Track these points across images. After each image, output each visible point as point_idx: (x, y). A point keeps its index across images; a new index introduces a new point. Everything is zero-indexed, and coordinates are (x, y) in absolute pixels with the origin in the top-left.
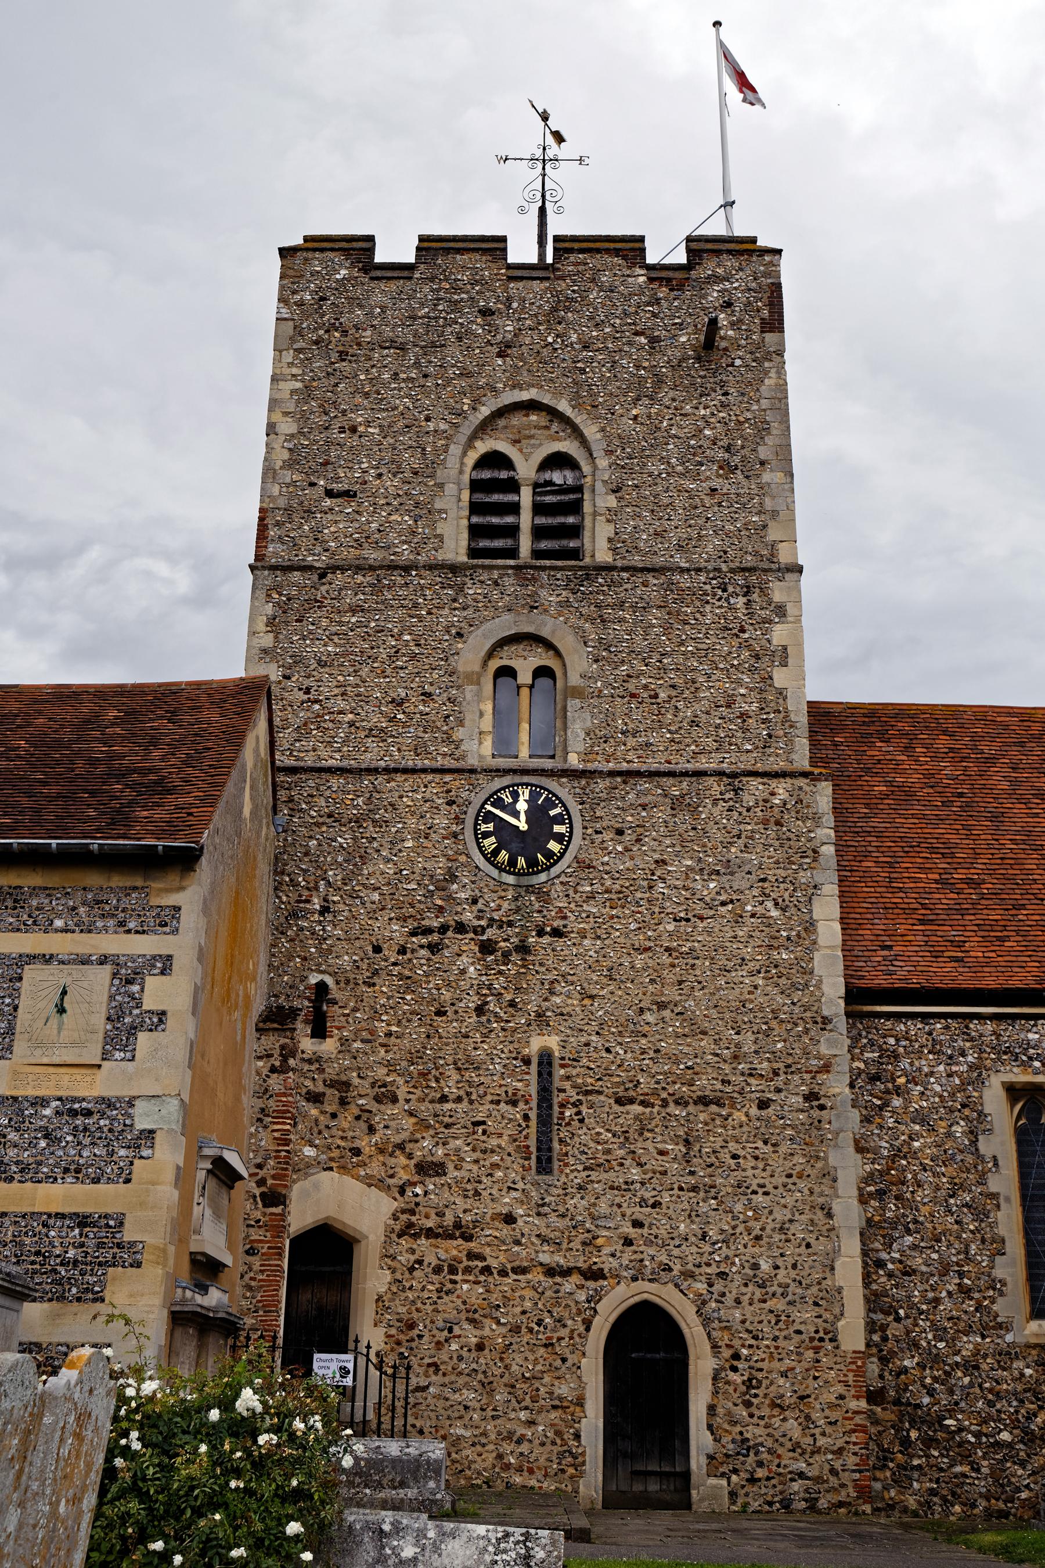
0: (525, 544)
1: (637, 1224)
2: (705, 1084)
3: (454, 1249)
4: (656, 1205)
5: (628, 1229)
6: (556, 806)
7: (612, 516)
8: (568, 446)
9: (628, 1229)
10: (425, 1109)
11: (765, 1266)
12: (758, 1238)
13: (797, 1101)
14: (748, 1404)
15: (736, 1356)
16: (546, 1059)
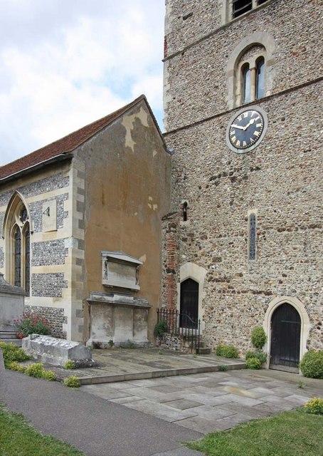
1: (284, 276)
2: (313, 220)
3: (223, 285)
5: (281, 278)
9: (281, 278)
10: (215, 240)
16: (253, 218)
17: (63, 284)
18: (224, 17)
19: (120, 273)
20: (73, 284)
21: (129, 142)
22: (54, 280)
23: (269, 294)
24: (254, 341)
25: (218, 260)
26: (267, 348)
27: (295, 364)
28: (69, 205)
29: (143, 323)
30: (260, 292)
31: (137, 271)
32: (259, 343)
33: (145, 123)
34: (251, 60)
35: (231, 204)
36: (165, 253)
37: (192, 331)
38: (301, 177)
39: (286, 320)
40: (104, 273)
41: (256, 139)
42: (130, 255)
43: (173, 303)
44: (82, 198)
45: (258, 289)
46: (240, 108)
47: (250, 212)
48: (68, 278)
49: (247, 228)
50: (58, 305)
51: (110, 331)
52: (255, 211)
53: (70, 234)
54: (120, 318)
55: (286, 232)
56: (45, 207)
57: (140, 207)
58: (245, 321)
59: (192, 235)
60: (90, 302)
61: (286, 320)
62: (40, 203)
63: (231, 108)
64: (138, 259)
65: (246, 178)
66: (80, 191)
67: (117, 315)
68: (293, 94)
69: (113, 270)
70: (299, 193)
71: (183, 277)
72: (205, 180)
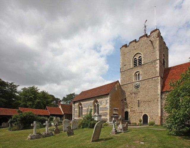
0: (138, 65)
3: (134, 112)
6: (157, 79)
7: (143, 60)
8: (140, 55)
10: (131, 104)
16: (139, 100)
17: (107, 114)
18: (132, 66)
20: (109, 114)
21: (116, 89)
22: (105, 114)
26: (142, 122)
27: (147, 124)
28: (108, 101)
32: (140, 121)
33: (118, 85)
34: (137, 74)
39: (145, 117)
41: (139, 87)
45: (140, 112)
48: (108, 113)
49: (138, 102)
50: (106, 118)
53: (109, 106)
56: (103, 102)
61: (145, 117)
62: (102, 101)
69: (115, 111)
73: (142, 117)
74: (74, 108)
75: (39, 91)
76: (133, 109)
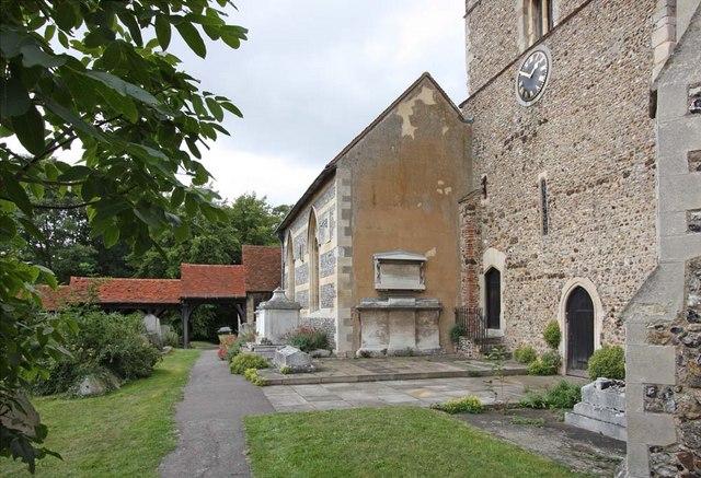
1: (576, 251)
2: (600, 174)
4: (582, 240)
5: (573, 254)
9: (573, 254)
11: (626, 263)
12: (623, 249)
13: (642, 167)
14: (617, 333)
15: (613, 310)
19: (395, 274)
23: (562, 276)
24: (546, 337)
25: (514, 241)
26: (563, 348)
29: (432, 326)
30: (555, 276)
31: (421, 269)
35: (523, 169)
36: (463, 242)
37: (491, 332)
38: (585, 121)
40: (376, 276)
42: (417, 253)
43: (473, 299)
44: (348, 205)
45: (552, 272)
46: (526, 51)
47: (540, 176)
51: (384, 338)
52: (543, 174)
54: (397, 323)
55: (575, 194)
57: (426, 196)
58: (542, 314)
59: (491, 214)
60: (360, 309)
63: (522, 50)
64: (424, 255)
65: (535, 135)
66: (345, 199)
67: (393, 328)
68: (574, 19)
69: (386, 272)
70: (585, 141)
71: (486, 267)
72: (499, 147)
73: (562, 306)
74: (293, 285)
75: (230, 205)
76: (519, 253)
